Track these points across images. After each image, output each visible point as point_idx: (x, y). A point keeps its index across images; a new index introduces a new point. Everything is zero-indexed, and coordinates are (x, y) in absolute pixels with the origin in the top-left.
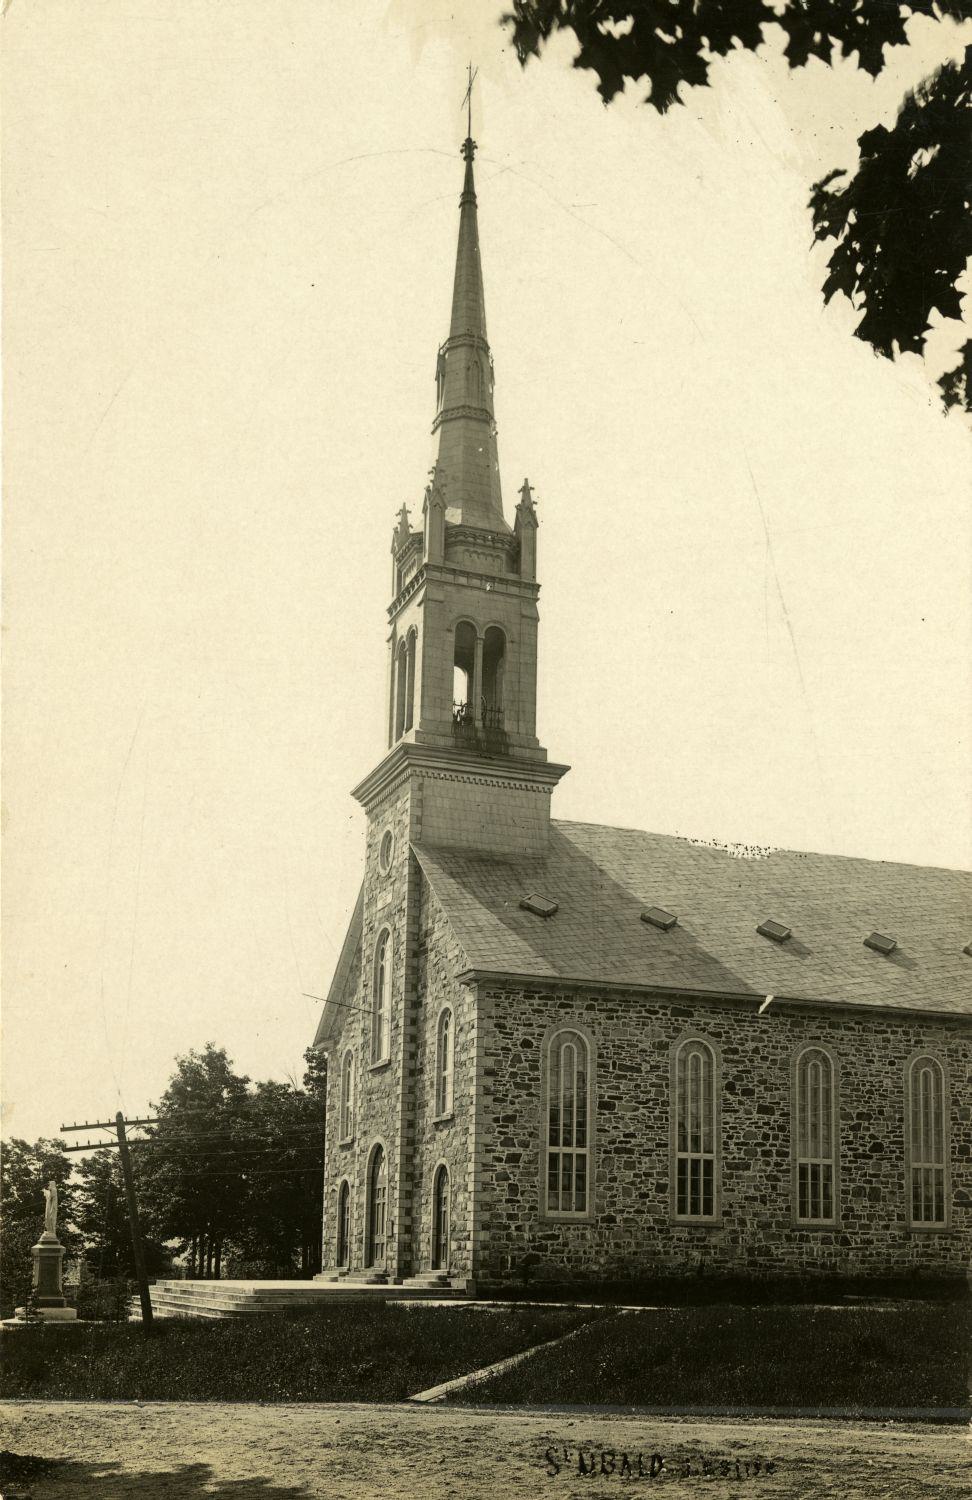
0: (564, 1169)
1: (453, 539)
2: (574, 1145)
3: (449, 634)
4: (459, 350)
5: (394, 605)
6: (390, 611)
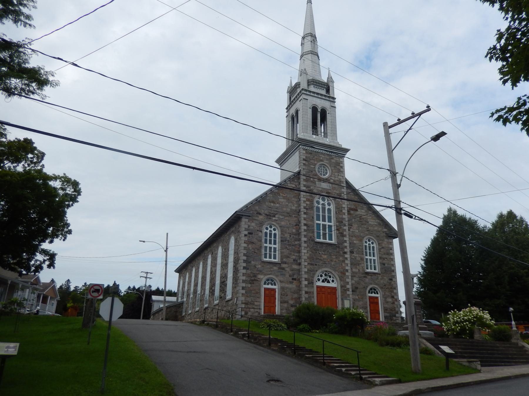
0: (326, 234)
1: (310, 83)
2: (327, 225)
3: (310, 109)
4: (309, 37)
5: (289, 106)
6: (287, 108)
